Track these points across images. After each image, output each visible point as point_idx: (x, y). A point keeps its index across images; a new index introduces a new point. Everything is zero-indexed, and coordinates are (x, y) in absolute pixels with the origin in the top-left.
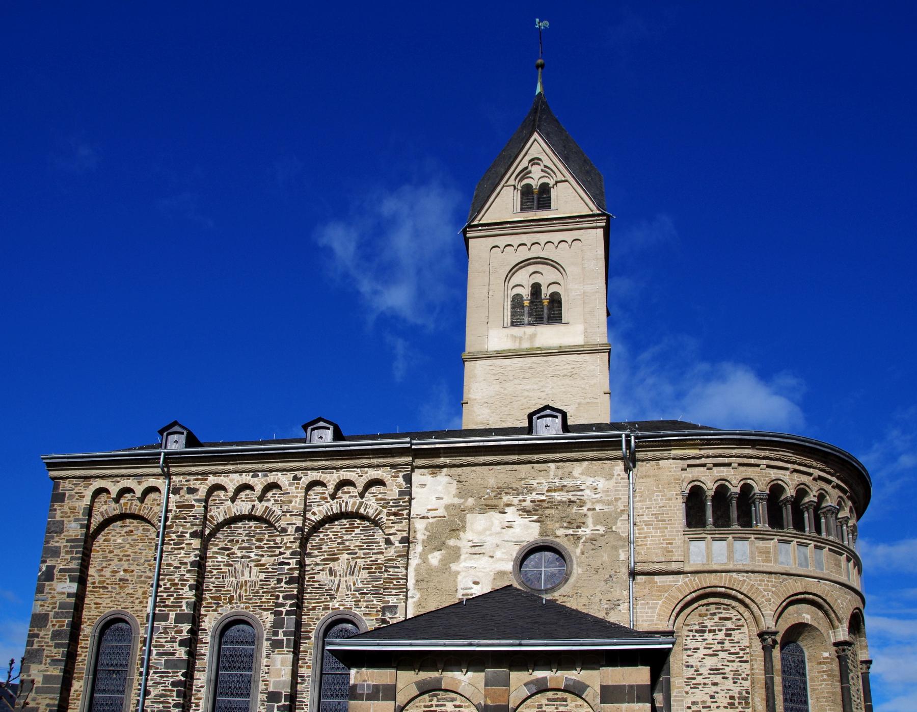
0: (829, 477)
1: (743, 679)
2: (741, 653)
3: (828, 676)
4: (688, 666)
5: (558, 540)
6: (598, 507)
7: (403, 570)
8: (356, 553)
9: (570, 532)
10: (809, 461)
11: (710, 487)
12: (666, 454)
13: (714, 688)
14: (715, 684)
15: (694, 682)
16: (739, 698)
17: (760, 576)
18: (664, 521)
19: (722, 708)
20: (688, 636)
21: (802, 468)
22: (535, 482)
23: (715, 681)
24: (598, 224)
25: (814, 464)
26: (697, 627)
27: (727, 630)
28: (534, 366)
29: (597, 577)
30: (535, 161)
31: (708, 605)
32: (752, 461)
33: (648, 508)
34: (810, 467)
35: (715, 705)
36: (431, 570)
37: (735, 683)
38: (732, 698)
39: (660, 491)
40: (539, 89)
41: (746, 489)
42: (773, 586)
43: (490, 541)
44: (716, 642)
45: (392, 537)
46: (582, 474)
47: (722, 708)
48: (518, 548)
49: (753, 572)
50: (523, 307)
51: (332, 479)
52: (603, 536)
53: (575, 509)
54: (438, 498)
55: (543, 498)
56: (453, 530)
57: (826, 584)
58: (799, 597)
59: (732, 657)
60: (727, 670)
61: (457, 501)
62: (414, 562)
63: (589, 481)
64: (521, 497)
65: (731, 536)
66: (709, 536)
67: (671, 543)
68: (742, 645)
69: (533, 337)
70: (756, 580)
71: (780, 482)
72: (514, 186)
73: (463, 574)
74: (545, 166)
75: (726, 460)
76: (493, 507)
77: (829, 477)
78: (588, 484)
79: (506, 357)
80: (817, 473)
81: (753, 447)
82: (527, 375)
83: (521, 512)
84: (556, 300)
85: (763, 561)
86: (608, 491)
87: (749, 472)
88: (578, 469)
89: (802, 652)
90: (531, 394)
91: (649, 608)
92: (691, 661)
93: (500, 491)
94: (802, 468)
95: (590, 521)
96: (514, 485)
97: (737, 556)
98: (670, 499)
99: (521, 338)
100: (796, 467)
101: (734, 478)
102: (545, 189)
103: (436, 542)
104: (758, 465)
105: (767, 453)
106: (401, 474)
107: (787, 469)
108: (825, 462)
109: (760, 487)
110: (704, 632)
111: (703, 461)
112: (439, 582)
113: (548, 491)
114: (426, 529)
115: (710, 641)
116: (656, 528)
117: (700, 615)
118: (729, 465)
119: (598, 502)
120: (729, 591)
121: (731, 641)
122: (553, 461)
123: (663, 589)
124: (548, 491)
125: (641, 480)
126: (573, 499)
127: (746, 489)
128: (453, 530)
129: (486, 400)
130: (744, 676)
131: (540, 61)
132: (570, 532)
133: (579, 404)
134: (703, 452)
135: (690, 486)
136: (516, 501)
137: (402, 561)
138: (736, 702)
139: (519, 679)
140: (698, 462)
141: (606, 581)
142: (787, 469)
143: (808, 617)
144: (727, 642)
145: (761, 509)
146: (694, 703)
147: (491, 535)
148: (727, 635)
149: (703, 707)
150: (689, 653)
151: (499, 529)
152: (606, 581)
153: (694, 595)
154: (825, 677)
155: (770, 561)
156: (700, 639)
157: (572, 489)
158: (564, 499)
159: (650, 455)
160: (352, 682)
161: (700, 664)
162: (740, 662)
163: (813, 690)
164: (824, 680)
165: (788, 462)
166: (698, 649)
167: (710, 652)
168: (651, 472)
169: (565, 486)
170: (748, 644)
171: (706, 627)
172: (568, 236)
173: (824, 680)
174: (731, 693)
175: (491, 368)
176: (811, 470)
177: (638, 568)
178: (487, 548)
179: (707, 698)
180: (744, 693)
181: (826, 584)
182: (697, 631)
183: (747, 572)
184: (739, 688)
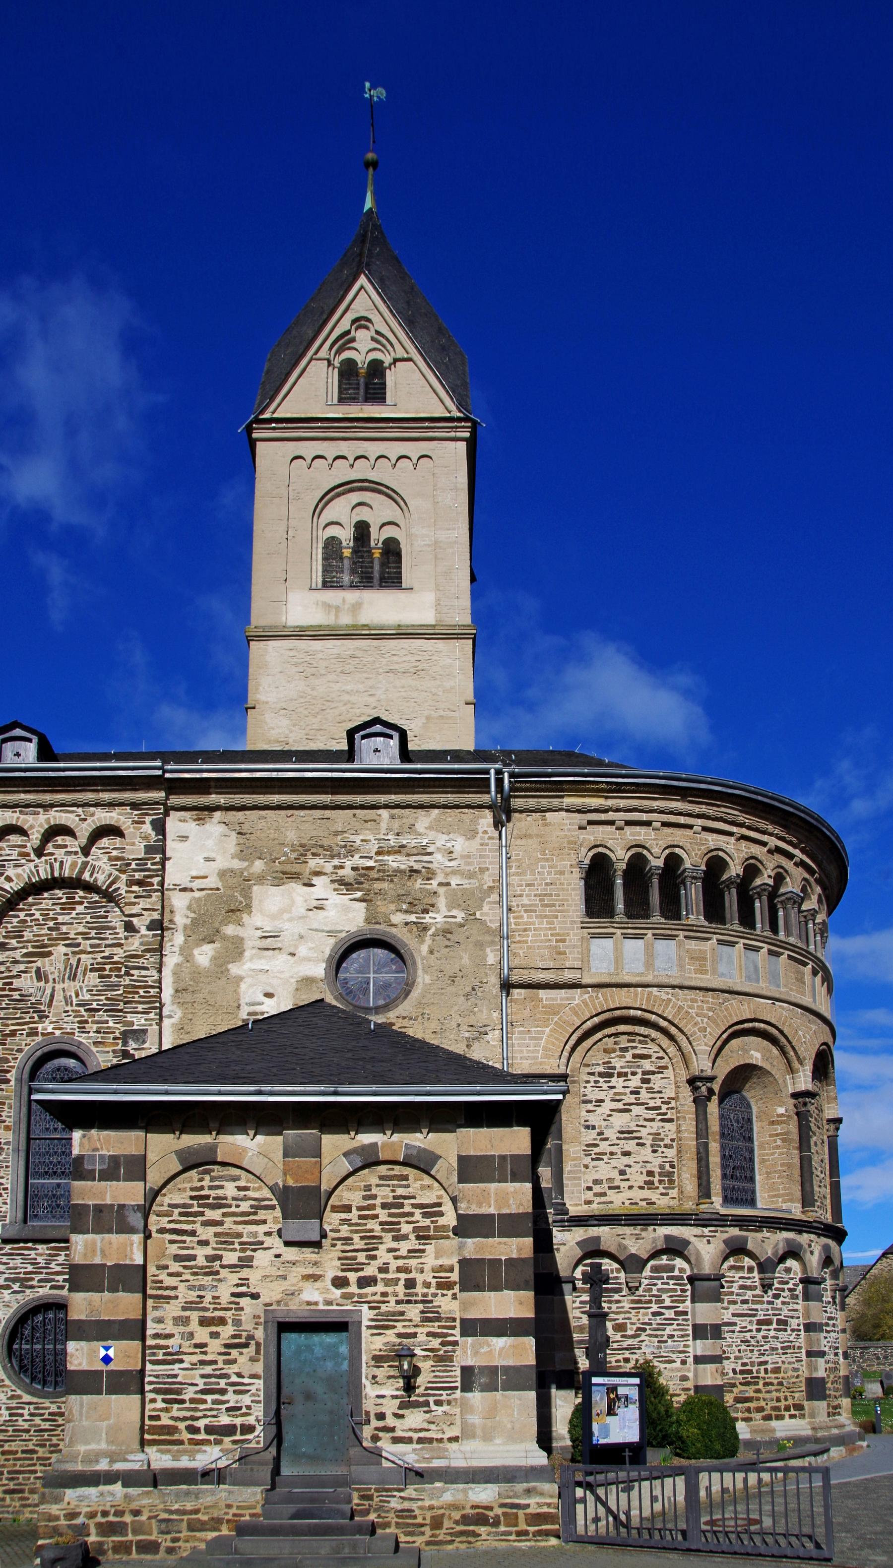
0: (790, 849)
1: (666, 1146)
2: (664, 1107)
3: (783, 1140)
4: (587, 1127)
5: (394, 930)
6: (454, 881)
7: (154, 973)
8: (79, 945)
9: (413, 918)
11: (620, 856)
12: (556, 802)
13: (626, 1160)
14: (627, 1154)
15: (596, 1150)
16: (660, 1174)
17: (691, 994)
18: (554, 905)
19: (636, 1188)
20: (588, 1082)
22: (358, 839)
23: (627, 1149)
24: (459, 435)
25: (770, 828)
26: (601, 1069)
27: (644, 1073)
28: (359, 653)
29: (452, 989)
30: (361, 322)
31: (616, 1035)
32: (682, 820)
33: (528, 885)
34: (764, 832)
35: (627, 1184)
36: (197, 973)
37: (654, 1151)
38: (650, 1173)
39: (547, 860)
41: (673, 861)
42: (710, 1009)
43: (290, 929)
44: (628, 1091)
45: (135, 920)
46: (430, 828)
48: (332, 941)
49: (681, 987)
50: (341, 558)
51: (37, 823)
52: (462, 926)
53: (419, 883)
54: (208, 859)
55: (371, 863)
56: (232, 911)
58: (746, 1025)
59: (651, 1114)
61: (237, 864)
62: (171, 960)
63: (441, 840)
64: (336, 862)
65: (650, 932)
66: (619, 932)
67: (564, 941)
68: (666, 1096)
69: (356, 607)
71: (721, 854)
72: (329, 361)
73: (248, 980)
74: (377, 333)
75: (644, 817)
76: (294, 876)
77: (790, 849)
78: (439, 844)
79: (315, 637)
80: (773, 842)
82: (348, 668)
83: (336, 886)
84: (392, 550)
85: (697, 971)
86: (469, 857)
88: (424, 820)
89: (749, 1106)
90: (353, 699)
91: (531, 1039)
92: (593, 1119)
93: (304, 850)
95: (442, 902)
96: (326, 843)
97: (658, 963)
98: (562, 873)
99: (338, 609)
101: (656, 844)
102: (377, 369)
103: (205, 929)
104: (690, 827)
105: (703, 809)
106: (148, 819)
107: (731, 834)
108: (785, 827)
109: (693, 860)
110: (611, 1075)
111: (611, 816)
112: (210, 993)
113: (378, 853)
114: (189, 908)
115: (619, 1089)
116: (541, 917)
117: (606, 1051)
118: (648, 824)
119: (454, 873)
120: (647, 1015)
121: (650, 1090)
122: (386, 807)
123: (553, 1010)
124: (378, 853)
125: (519, 842)
126: (416, 867)
127: (673, 861)
128: (232, 911)
129: (284, 705)
130: (667, 1141)
132: (413, 918)
133: (428, 718)
134: (610, 803)
135: (591, 854)
136: (328, 868)
137: (151, 960)
138: (656, 1179)
139: (335, 1145)
140: (603, 817)
141: (467, 995)
142: (731, 834)
144: (643, 1092)
145: (693, 893)
146: (596, 1182)
147: (290, 920)
148: (645, 1081)
149: (610, 1188)
150: (590, 1107)
151: (303, 911)
152: (467, 995)
153: (596, 1020)
154: (779, 1142)
155: (705, 972)
156: (605, 1086)
157: (415, 851)
158: (403, 867)
159: (532, 803)
160: (76, 1151)
161: (604, 1124)
162: (662, 1120)
163: (763, 1161)
164: (778, 1147)
166: (603, 1101)
167: (620, 1106)
168: (534, 830)
169: (403, 846)
170: (673, 1095)
171: (614, 1068)
172: (413, 449)
173: (778, 1147)
174: (649, 1167)
175: (292, 653)
176: (765, 838)
177: (515, 978)
178: (285, 940)
179: (615, 1174)
180: (667, 1167)
181: (783, 1008)
182: (601, 1075)
183: (673, 987)
184: (660, 1160)
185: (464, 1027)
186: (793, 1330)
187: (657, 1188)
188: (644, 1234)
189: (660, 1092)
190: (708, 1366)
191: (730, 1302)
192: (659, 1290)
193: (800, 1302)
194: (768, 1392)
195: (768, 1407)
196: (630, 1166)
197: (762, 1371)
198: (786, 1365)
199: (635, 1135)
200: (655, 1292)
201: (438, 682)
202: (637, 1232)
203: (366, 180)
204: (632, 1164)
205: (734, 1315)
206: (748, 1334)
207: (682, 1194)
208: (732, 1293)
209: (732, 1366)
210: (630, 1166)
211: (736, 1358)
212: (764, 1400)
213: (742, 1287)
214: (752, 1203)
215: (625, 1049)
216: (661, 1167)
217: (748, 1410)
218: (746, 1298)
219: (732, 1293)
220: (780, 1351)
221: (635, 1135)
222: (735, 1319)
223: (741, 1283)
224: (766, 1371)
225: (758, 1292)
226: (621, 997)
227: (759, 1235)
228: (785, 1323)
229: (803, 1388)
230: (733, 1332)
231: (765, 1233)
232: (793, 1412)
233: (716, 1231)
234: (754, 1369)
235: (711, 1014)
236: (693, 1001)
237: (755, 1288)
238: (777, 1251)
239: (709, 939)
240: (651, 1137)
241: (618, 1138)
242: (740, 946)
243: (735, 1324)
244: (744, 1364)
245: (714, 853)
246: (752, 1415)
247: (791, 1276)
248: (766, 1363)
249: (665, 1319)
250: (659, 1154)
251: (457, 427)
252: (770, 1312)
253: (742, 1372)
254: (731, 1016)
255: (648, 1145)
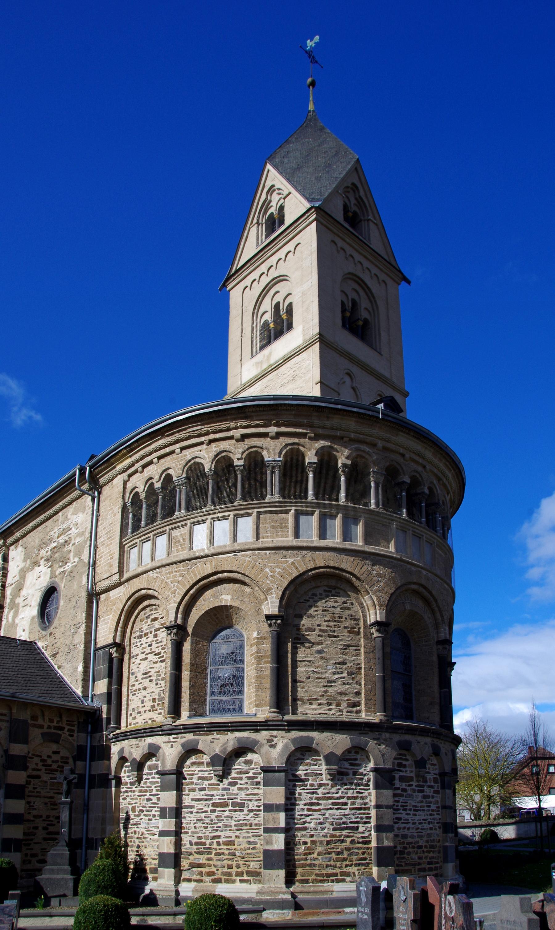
0: (261, 430)
2: (163, 651)
10: (224, 425)
12: (114, 472)
13: (144, 693)
14: (145, 688)
19: (147, 711)
21: (218, 436)
24: (311, 220)
25: (233, 424)
31: (144, 608)
32: (167, 450)
34: (229, 429)
38: (154, 700)
40: (311, 107)
47: (147, 711)
57: (246, 556)
58: (212, 578)
60: (153, 671)
66: (138, 540)
70: (166, 574)
77: (261, 430)
81: (163, 436)
87: (166, 462)
89: (241, 635)
94: (218, 436)
100: (212, 436)
104: (173, 452)
105: (177, 436)
107: (202, 443)
108: (246, 418)
126: (67, 538)
131: (309, 80)
138: (156, 704)
142: (202, 443)
143: (229, 597)
144: (154, 643)
145: (274, 480)
148: (155, 636)
156: (139, 644)
159: (106, 477)
161: (137, 670)
165: (200, 436)
166: (137, 655)
167: (144, 656)
172: (290, 246)
176: (231, 433)
177: (99, 587)
181: (246, 556)
185: (72, 626)
186: (251, 811)
187: (156, 710)
188: (140, 743)
189: (161, 642)
190: (165, 838)
191: (190, 790)
192: (150, 782)
193: (262, 787)
194: (219, 860)
195: (220, 872)
196: (145, 697)
197: (215, 843)
198: (241, 839)
199: (149, 674)
200: (148, 784)
201: (303, 379)
202: (137, 742)
203: (309, 93)
204: (146, 695)
205: (193, 800)
206: (204, 815)
207: (160, 717)
208: (192, 783)
209: (190, 839)
210: (145, 697)
211: (193, 833)
212: (215, 866)
213: (200, 778)
214: (241, 709)
215: (148, 617)
216: (159, 694)
217: (201, 874)
218: (204, 786)
219: (192, 783)
220: (234, 828)
221: (149, 674)
222: (193, 803)
223: (200, 775)
224: (218, 844)
225: (214, 781)
226: (136, 584)
227: (210, 738)
228: (242, 805)
229: (261, 858)
230: (191, 812)
231: (215, 735)
232: (245, 877)
233: (177, 738)
234: (208, 842)
235: (181, 578)
236: (170, 573)
237: (211, 778)
238: (225, 749)
239: (186, 525)
240: (155, 674)
241: (143, 679)
242: (208, 521)
243: (192, 807)
244: (199, 838)
245: (193, 462)
246: (204, 878)
247: (253, 766)
248: (219, 837)
249: (153, 803)
250: (159, 686)
251: (308, 216)
252: (226, 797)
253: (197, 844)
254: (195, 575)
255: (154, 681)
